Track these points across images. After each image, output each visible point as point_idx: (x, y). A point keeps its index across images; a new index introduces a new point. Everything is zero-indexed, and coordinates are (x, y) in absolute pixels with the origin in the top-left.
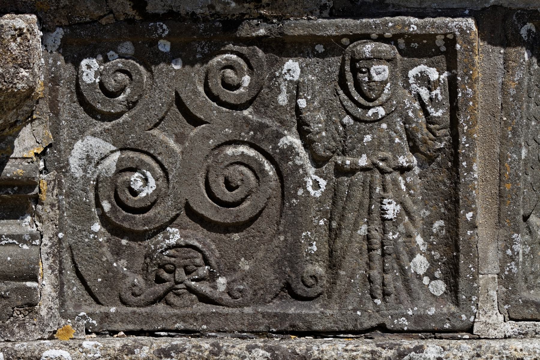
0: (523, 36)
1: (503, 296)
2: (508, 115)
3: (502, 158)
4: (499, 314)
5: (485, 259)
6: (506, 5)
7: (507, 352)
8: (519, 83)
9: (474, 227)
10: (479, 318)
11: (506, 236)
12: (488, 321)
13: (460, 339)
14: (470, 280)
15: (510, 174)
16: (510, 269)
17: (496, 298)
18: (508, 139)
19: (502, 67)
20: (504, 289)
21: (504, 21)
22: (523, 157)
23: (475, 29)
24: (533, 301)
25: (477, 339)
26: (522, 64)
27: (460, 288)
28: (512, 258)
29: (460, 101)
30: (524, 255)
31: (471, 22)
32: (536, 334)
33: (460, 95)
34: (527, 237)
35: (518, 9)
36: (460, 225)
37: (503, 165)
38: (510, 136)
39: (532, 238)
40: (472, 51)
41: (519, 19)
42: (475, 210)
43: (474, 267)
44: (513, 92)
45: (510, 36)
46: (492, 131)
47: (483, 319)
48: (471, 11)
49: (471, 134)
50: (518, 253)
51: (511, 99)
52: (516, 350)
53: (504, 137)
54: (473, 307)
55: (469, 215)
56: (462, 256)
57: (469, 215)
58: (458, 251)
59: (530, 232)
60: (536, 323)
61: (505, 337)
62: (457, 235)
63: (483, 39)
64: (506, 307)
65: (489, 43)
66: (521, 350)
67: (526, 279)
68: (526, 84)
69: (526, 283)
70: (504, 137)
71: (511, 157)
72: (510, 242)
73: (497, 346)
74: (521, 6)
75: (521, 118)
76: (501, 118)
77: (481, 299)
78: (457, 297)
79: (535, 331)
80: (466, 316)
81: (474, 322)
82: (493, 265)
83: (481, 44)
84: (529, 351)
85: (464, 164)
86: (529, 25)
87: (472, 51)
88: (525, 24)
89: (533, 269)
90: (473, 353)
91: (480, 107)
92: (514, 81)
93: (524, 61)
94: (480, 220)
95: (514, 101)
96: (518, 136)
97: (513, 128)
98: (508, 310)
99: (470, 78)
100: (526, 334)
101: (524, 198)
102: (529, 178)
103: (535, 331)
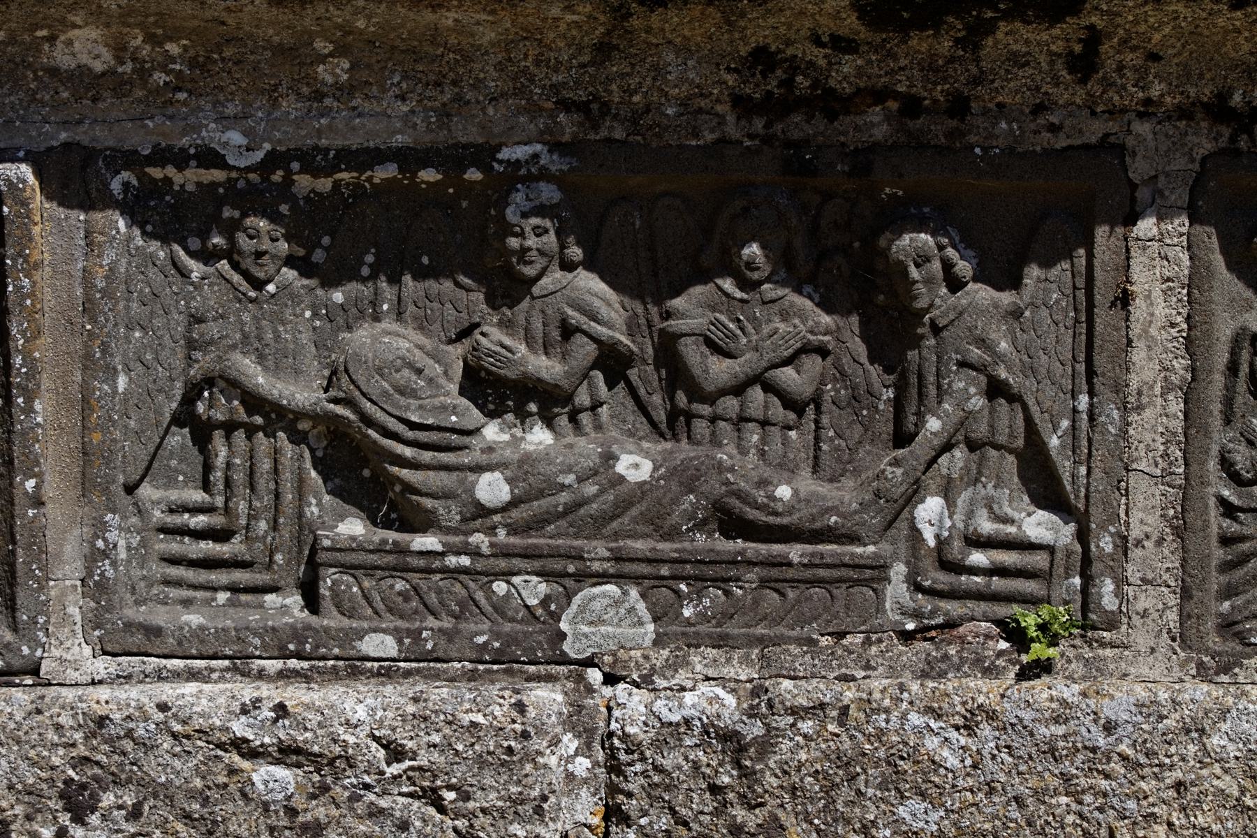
0: (115, 192)
1: (90, 615)
2: (93, 320)
3: (86, 390)
4: (84, 645)
5: (58, 555)
6: (86, 143)
7: (84, 705)
8: (110, 269)
9: (38, 502)
10: (49, 652)
11: (94, 518)
12: (65, 656)
13: (18, 685)
14: (33, 590)
15: (99, 417)
16: (103, 572)
17: (78, 619)
18: (95, 364)
19: (82, 243)
20: (93, 604)
21: (83, 168)
22: (121, 390)
23: (31, 179)
24: (140, 624)
25: (46, 685)
26: (114, 238)
27: (19, 602)
28: (104, 554)
29: (12, 298)
30: (129, 548)
31: (26, 170)
32: (146, 676)
33: (10, 288)
34: (134, 520)
35: (106, 149)
36: (17, 501)
37: (88, 403)
38: (98, 355)
39: (142, 521)
40: (28, 217)
41: (107, 165)
42: (39, 476)
43: (40, 569)
44: (100, 284)
45: (94, 194)
46: (68, 347)
47: (56, 653)
48: (28, 152)
49: (30, 352)
50: (115, 546)
51: (98, 295)
52: (98, 702)
53: (88, 356)
54: (41, 634)
55: (30, 484)
56: (20, 552)
57: (30, 484)
58: (14, 542)
59: (139, 511)
60: (146, 659)
61: (93, 683)
62: (13, 517)
63: (50, 198)
64: (97, 633)
65: (60, 205)
66: (107, 702)
67: (134, 588)
68: (123, 270)
69: (133, 594)
70: (88, 356)
71: (100, 389)
72: (100, 528)
73: (70, 696)
74: (111, 143)
75: (116, 325)
76: (83, 326)
77: (53, 620)
78: (14, 618)
79: (143, 672)
80: (30, 648)
81: (42, 658)
82: (74, 565)
83: (47, 206)
84: (118, 704)
85: (20, 400)
86: (125, 175)
87: (28, 217)
88: (118, 172)
89: (145, 572)
90: (31, 707)
91: (46, 309)
92: (101, 266)
93: (118, 232)
94: (49, 492)
95: (102, 298)
96: (111, 355)
97: (103, 343)
98: (100, 639)
99: (26, 261)
100: (128, 678)
101: (124, 457)
102: (132, 423)
103: (143, 672)
